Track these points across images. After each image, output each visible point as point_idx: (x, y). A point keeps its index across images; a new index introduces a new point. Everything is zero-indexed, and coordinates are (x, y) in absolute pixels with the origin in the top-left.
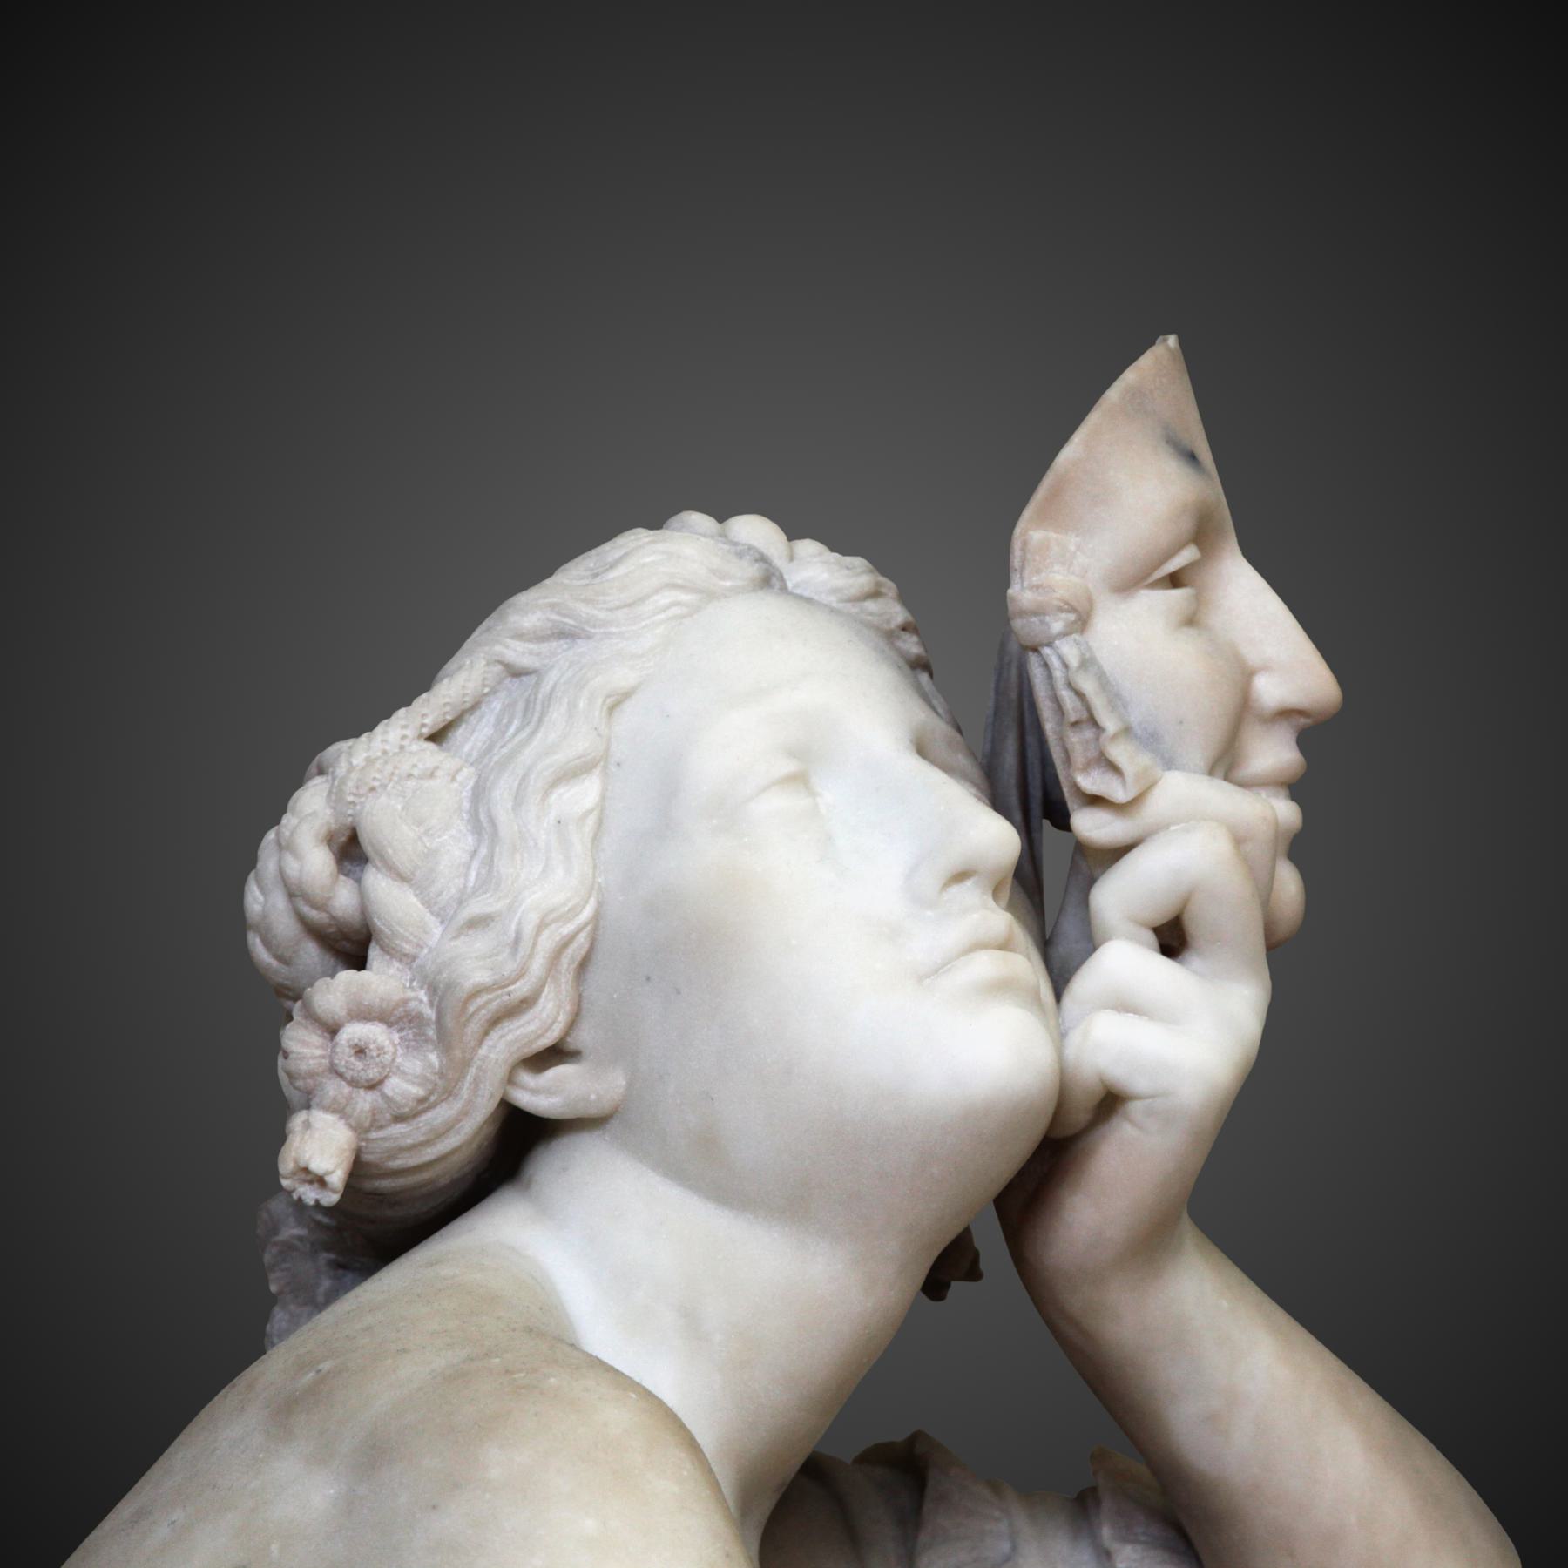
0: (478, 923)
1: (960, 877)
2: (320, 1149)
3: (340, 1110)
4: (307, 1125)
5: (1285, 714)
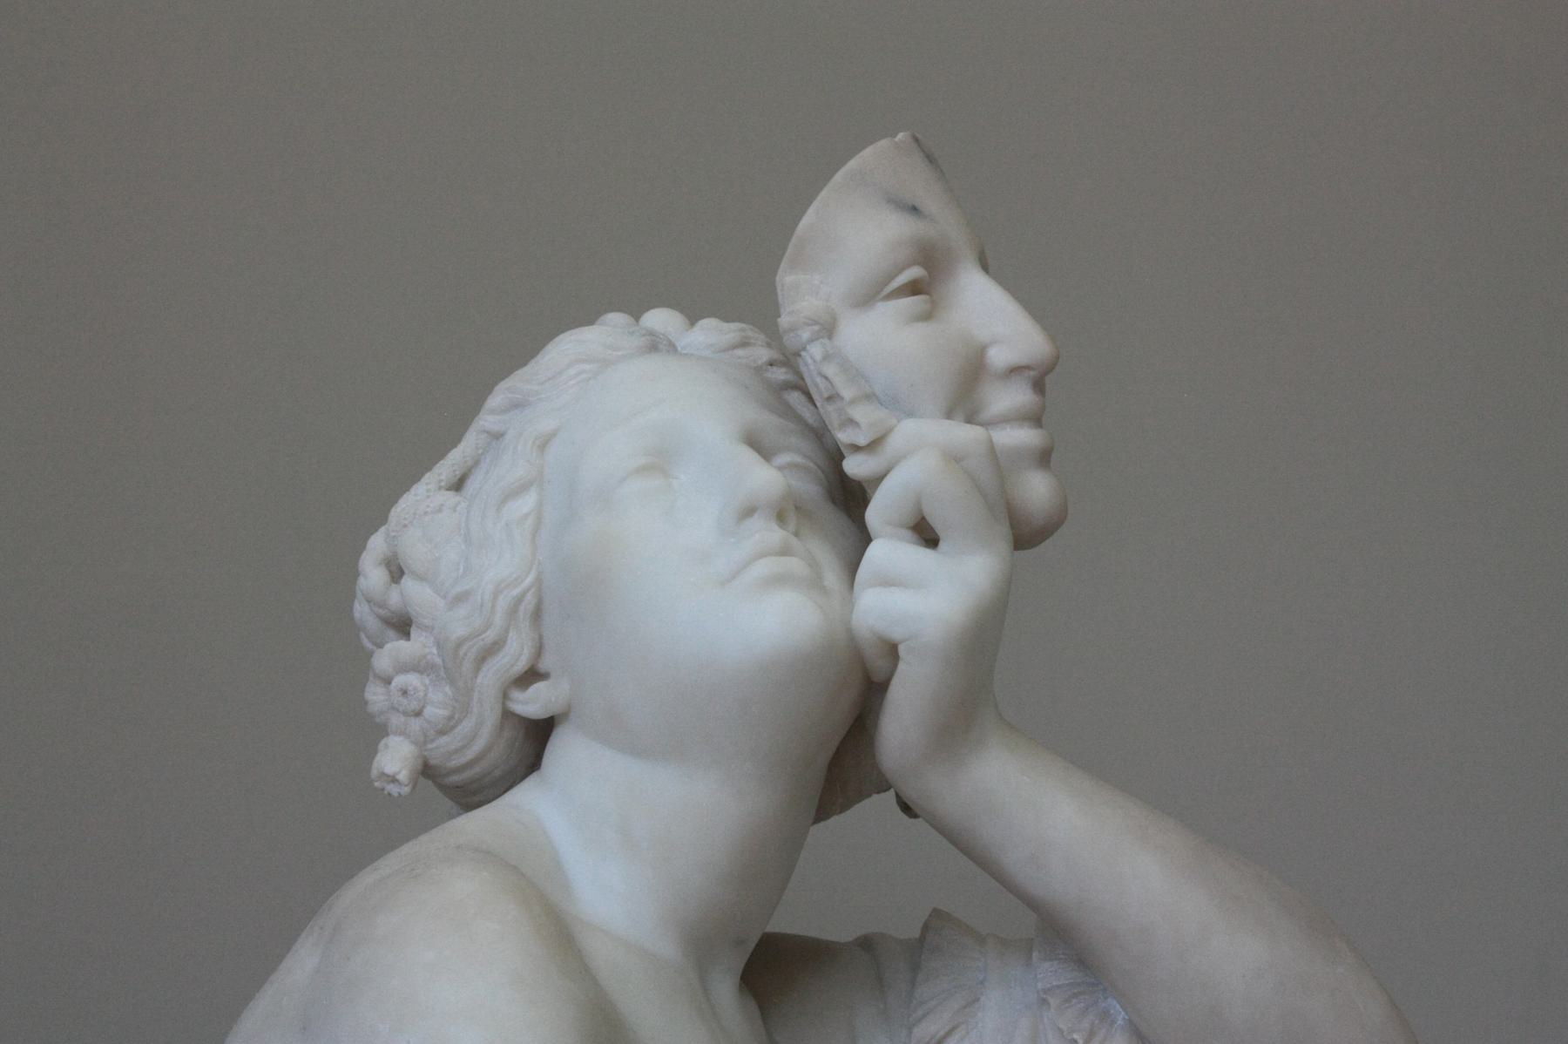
0: (461, 598)
1: (748, 512)
2: (395, 759)
3: (402, 733)
4: (387, 746)
5: (1015, 371)
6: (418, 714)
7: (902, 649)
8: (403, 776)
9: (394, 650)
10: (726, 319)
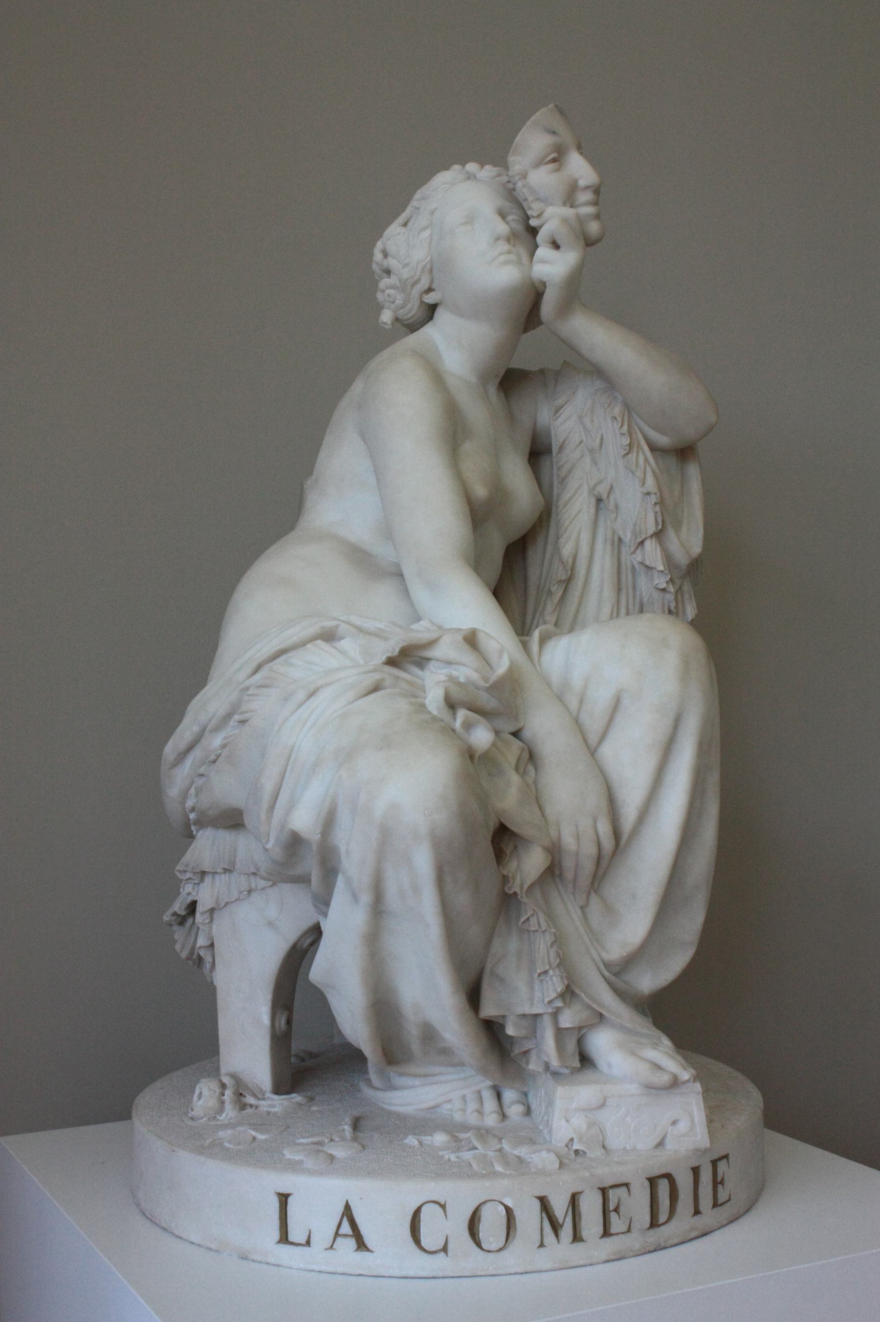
0: (406, 265)
1: (498, 239)
2: (386, 317)
3: (389, 308)
5: (587, 188)
6: (393, 302)
7: (547, 284)
8: (389, 322)
9: (385, 282)
10: (495, 166)
